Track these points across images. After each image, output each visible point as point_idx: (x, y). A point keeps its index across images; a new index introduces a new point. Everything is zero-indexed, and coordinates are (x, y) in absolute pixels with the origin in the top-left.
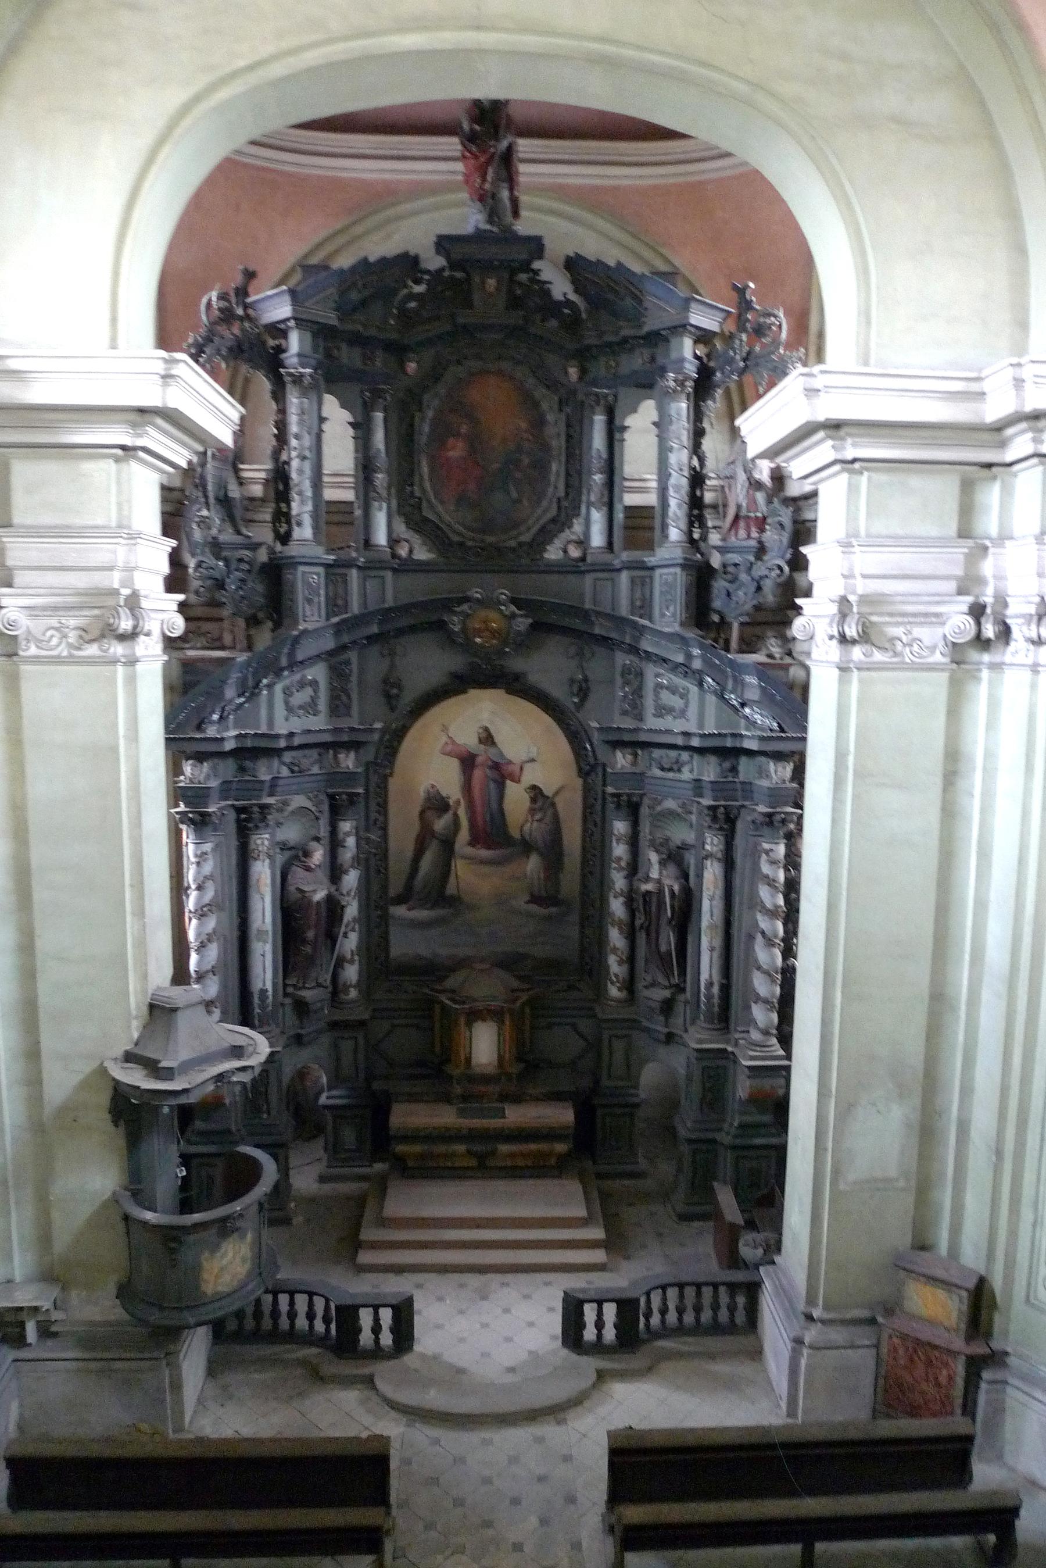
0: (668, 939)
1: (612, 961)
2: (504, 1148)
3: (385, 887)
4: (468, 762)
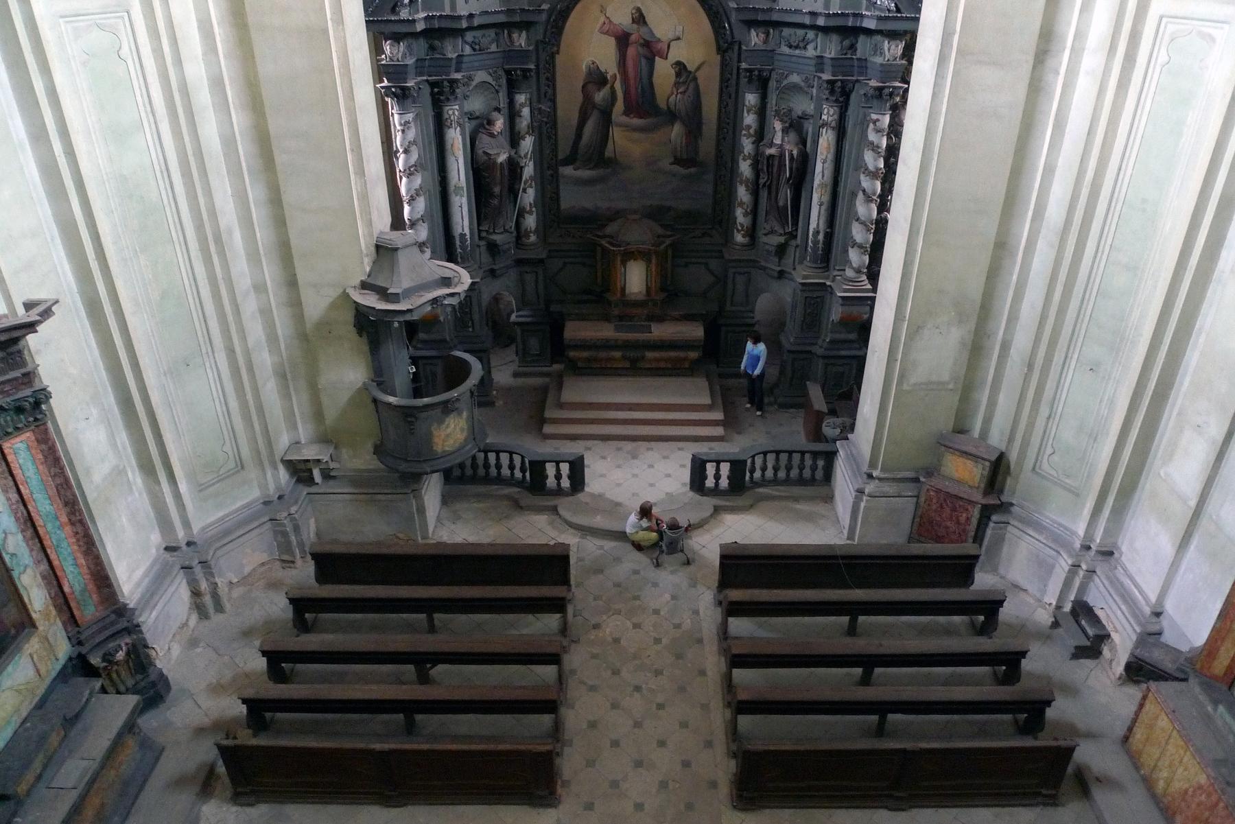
0: (786, 194)
1: (739, 212)
2: (650, 355)
3: (555, 150)
4: (623, 40)
